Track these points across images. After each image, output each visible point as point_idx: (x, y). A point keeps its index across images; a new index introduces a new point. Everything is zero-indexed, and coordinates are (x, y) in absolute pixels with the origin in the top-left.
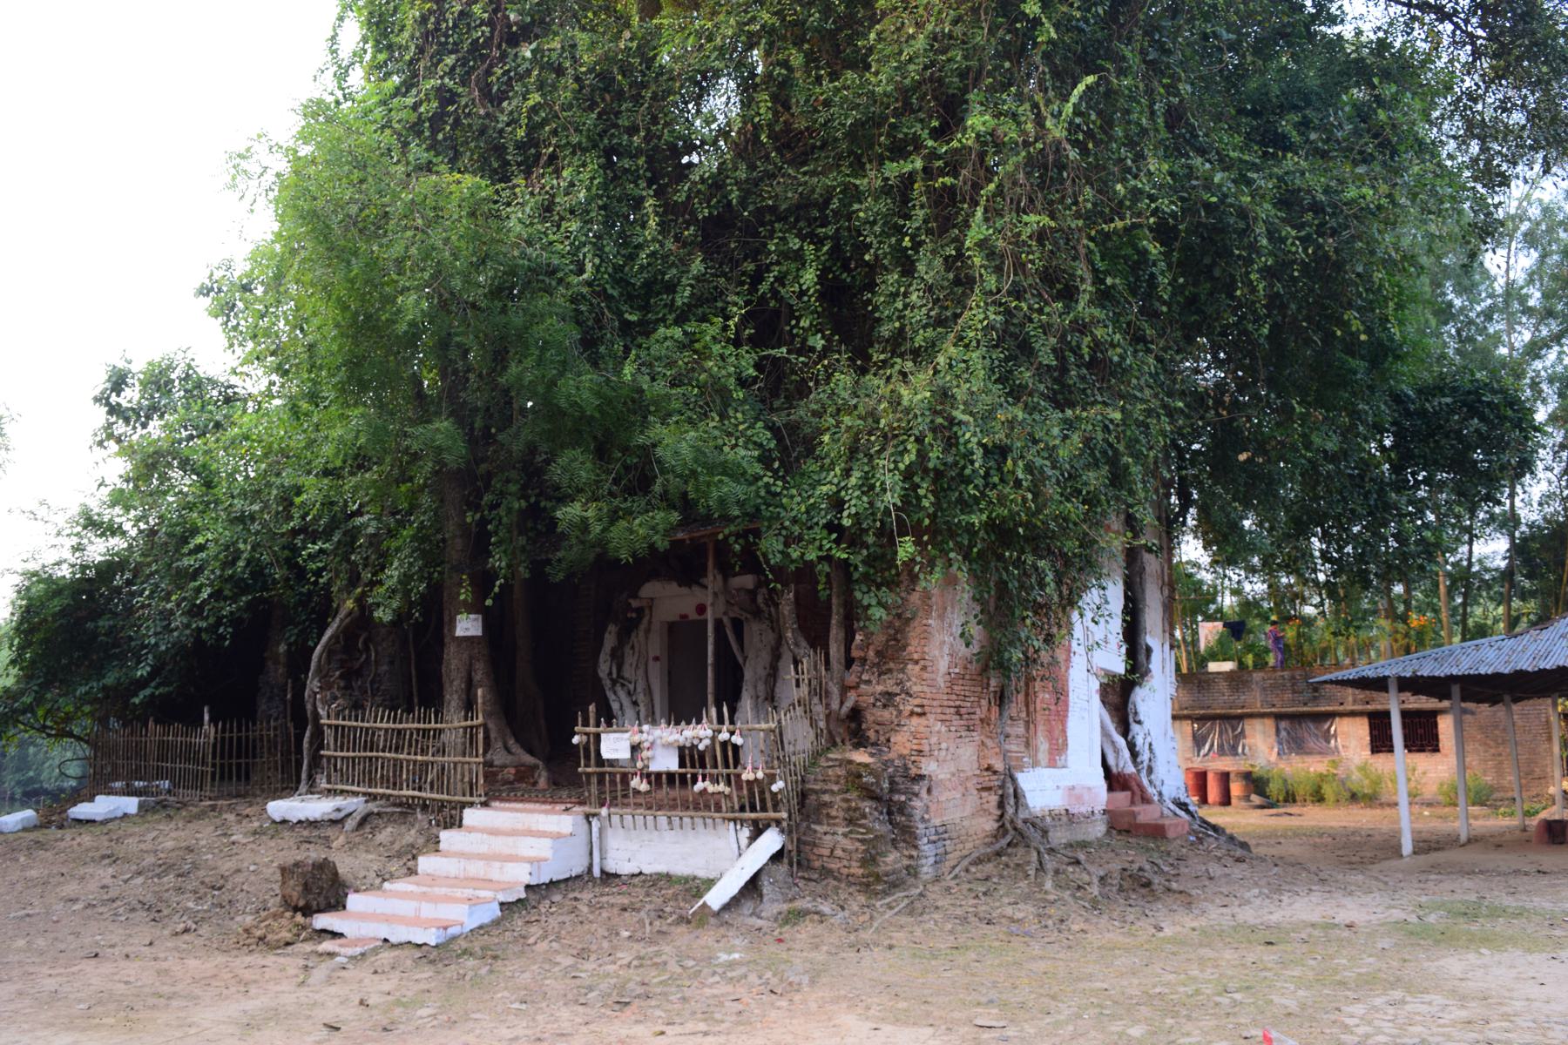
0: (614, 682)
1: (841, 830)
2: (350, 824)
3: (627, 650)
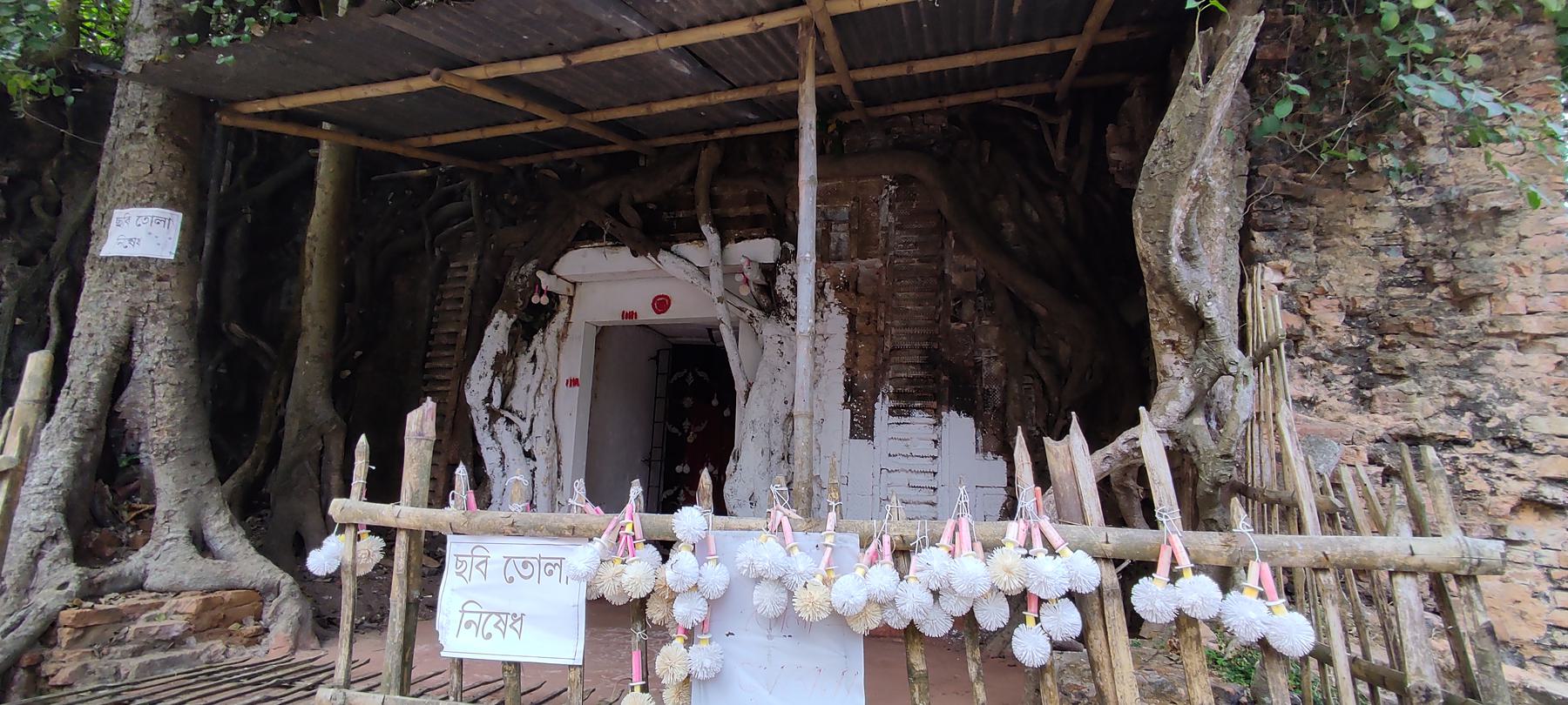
0: (494, 415)
3: (523, 362)
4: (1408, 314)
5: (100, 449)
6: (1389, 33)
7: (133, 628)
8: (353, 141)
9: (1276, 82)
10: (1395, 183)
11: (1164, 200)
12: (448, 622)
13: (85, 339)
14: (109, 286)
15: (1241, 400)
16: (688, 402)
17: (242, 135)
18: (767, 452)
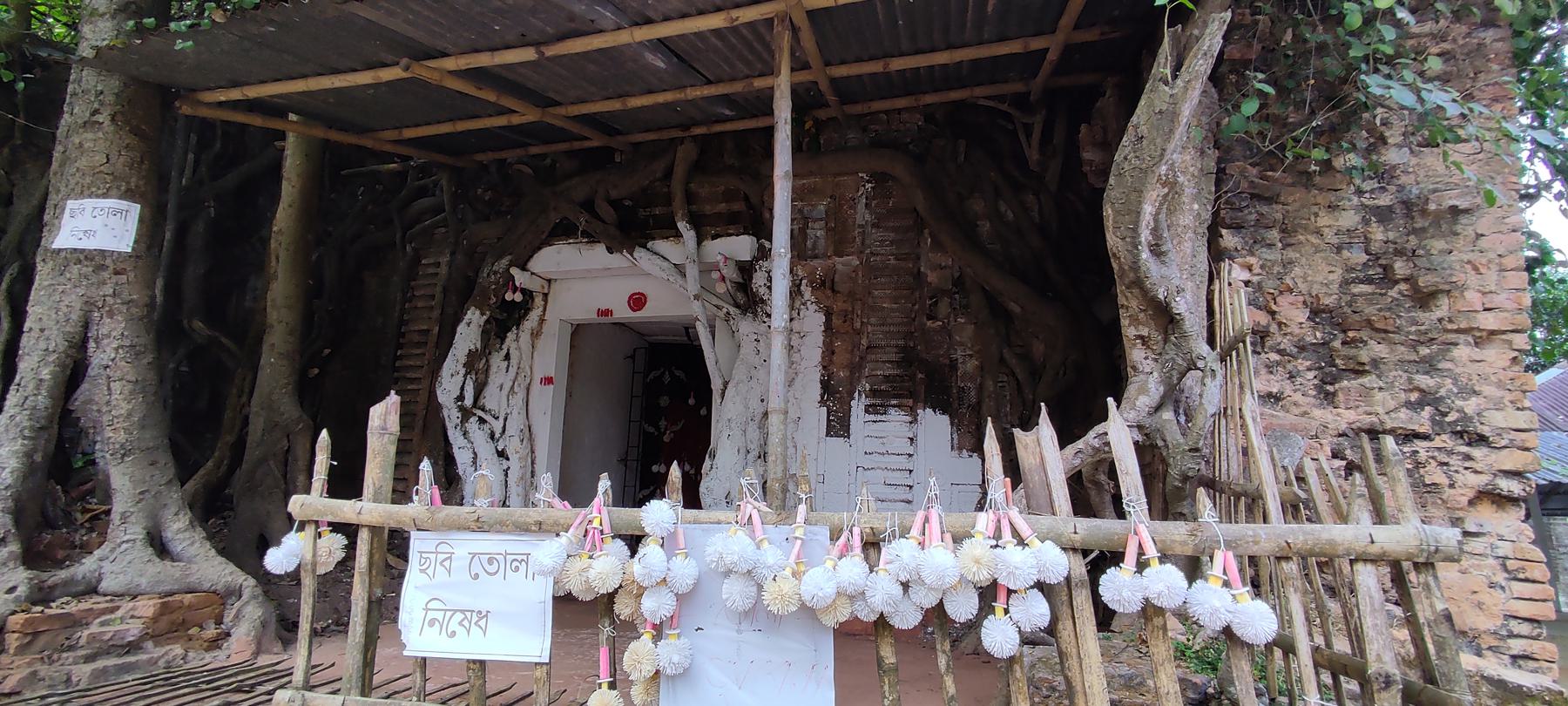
0: (466, 414)
3: (497, 360)
4: (1370, 311)
5: (52, 447)
6: (1352, 34)
7: (86, 633)
8: (320, 133)
9: (1243, 82)
10: (1358, 181)
11: (1133, 196)
12: (411, 620)
13: (35, 334)
14: (62, 279)
15: (1208, 394)
16: (664, 401)
17: (206, 125)
18: (743, 451)
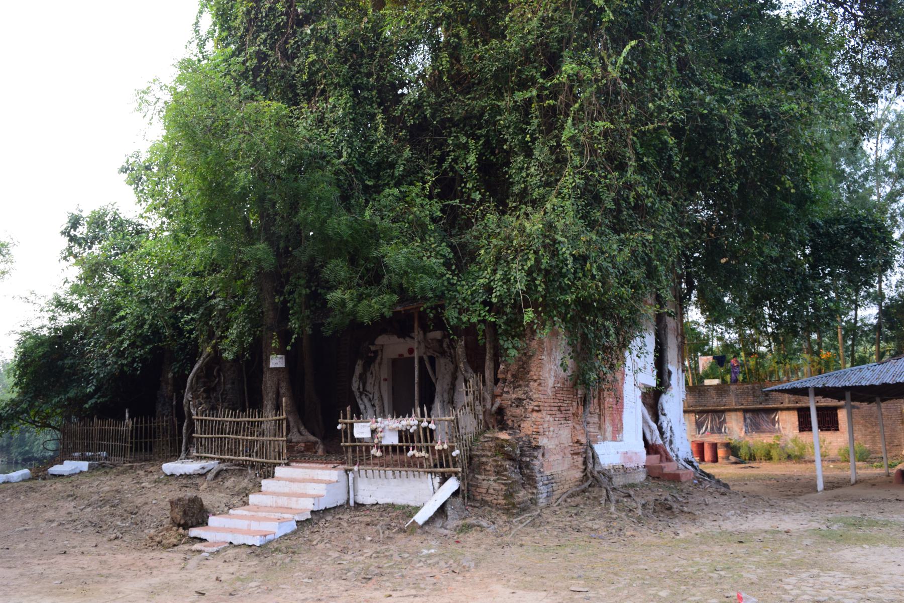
0: (361, 394)
1: (492, 478)
2: (210, 476)
3: (369, 375)
